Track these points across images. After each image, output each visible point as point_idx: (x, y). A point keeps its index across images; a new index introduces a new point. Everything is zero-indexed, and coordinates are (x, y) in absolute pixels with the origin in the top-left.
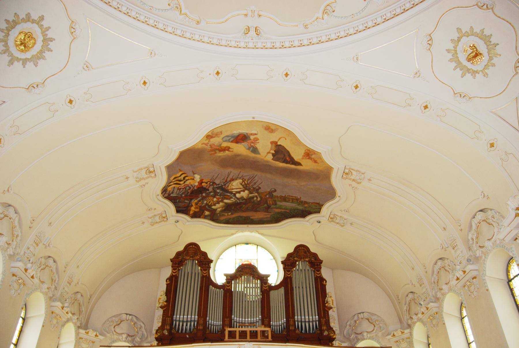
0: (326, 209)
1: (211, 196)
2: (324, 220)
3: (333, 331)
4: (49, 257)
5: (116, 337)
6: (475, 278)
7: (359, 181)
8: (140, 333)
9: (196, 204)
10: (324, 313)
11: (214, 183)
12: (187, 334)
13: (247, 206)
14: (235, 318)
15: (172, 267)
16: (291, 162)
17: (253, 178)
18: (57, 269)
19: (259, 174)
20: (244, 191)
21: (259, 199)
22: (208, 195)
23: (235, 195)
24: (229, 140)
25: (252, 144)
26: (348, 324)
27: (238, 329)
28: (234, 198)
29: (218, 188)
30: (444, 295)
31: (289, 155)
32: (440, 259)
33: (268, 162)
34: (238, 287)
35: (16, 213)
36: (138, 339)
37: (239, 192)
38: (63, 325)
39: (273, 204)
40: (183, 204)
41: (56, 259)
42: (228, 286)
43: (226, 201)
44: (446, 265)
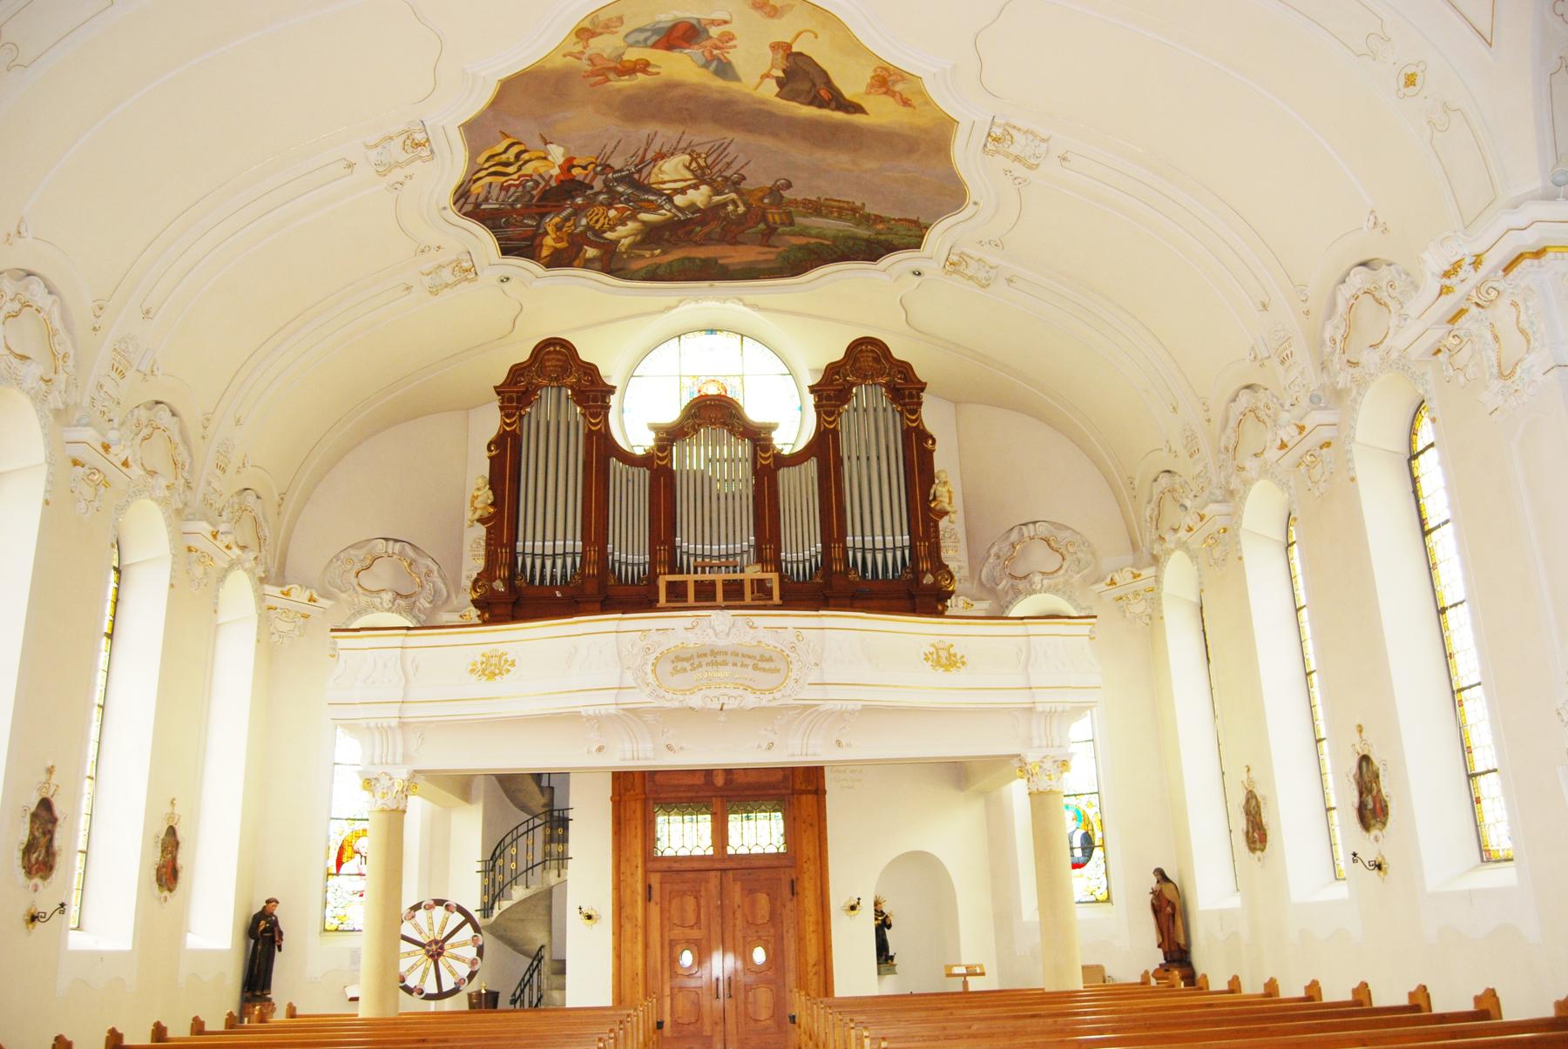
0: (935, 238)
1: (602, 204)
2: (932, 268)
3: (950, 573)
4: (158, 403)
5: (364, 600)
6: (1328, 444)
7: (1033, 161)
8: (429, 586)
9: (558, 228)
10: (926, 531)
11: (607, 167)
12: (556, 588)
13: (707, 229)
14: (686, 543)
15: (502, 408)
16: (833, 104)
17: (722, 149)
18: (183, 433)
19: (739, 138)
20: (696, 187)
21: (741, 209)
22: (591, 202)
23: (670, 199)
24: (646, 40)
25: (716, 52)
26: (993, 552)
27: (690, 579)
28: (667, 206)
29: (620, 181)
30: (1247, 483)
31: (828, 82)
32: (1248, 387)
33: (763, 102)
34: (692, 458)
35: (50, 293)
36: (424, 603)
37: (683, 191)
38: (221, 579)
39: (783, 224)
40: (519, 230)
41: (179, 408)
42: (662, 459)
43: (644, 216)
44: (1260, 404)
